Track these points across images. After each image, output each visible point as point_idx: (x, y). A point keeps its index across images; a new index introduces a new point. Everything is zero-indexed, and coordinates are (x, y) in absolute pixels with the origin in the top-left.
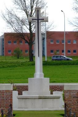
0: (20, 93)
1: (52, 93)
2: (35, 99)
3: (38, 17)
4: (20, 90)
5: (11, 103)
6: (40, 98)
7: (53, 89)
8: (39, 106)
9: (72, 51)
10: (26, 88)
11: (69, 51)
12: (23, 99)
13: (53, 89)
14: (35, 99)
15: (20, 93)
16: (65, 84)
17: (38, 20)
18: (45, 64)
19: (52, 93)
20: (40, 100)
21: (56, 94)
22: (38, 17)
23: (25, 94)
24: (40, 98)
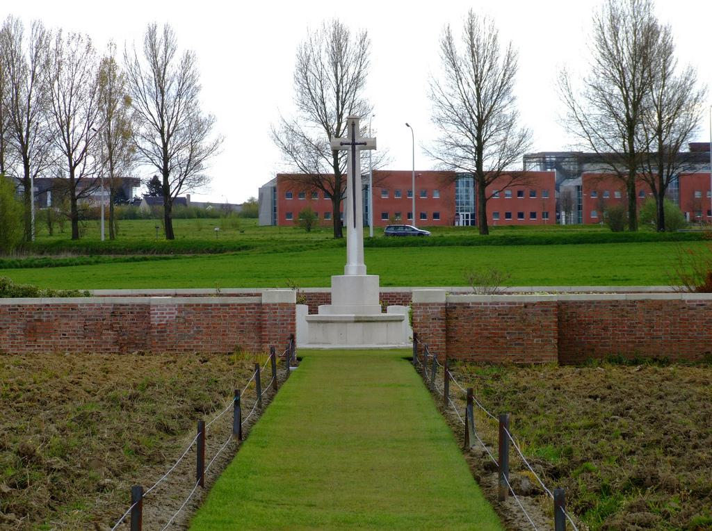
0: (313, 310)
1: (384, 310)
2: (346, 322)
4: (313, 303)
7: (387, 300)
8: (355, 339)
10: (326, 299)
11: (423, 216)
12: (319, 322)
14: (346, 322)
15: (313, 310)
17: (354, 144)
19: (384, 310)
23: (324, 312)
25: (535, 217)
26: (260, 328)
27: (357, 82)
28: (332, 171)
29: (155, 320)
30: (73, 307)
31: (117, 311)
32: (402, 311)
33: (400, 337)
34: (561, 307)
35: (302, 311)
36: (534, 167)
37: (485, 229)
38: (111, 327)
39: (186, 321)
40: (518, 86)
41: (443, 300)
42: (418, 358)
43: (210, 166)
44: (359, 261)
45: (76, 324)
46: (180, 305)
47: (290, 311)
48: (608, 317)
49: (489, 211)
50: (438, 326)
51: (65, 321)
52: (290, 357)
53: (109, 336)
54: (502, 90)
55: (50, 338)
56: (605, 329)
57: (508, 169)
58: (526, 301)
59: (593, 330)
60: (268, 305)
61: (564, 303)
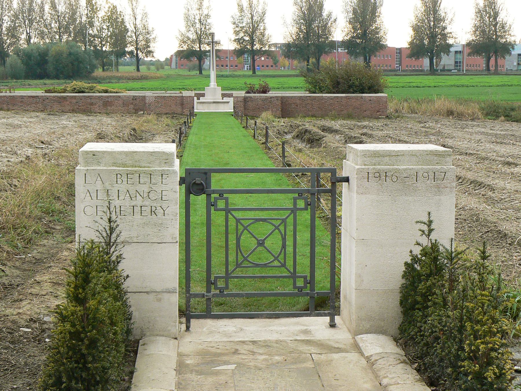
0: (198, 99)
1: (223, 99)
2: (210, 103)
3: (213, 40)
4: (199, 96)
5: (68, 178)
6: (214, 103)
7: (224, 95)
8: (213, 109)
9: (234, 65)
10: (203, 95)
11: (232, 66)
12: (201, 103)
13: (224, 95)
14: (210, 103)
15: (198, 99)
16: (43, 94)
17: (213, 42)
18: (218, 76)
19: (223, 99)
20: (148, 290)
21: (226, 99)
22: (213, 40)
23: (202, 99)
24: (214, 103)
25: (513, 337)
26: (182, 104)
27: (207, 16)
28: (198, 49)
29: (147, 101)
30: (119, 97)
31: (135, 98)
32: (231, 100)
33: (229, 108)
34: (282, 98)
35: (195, 98)
36: (273, 49)
37: (254, 72)
38: (132, 103)
39: (158, 102)
40: (268, 19)
41: (244, 96)
42: (235, 114)
43: (153, 46)
44: (214, 82)
45: (120, 102)
46: (155, 96)
47: (193, 98)
48: (298, 102)
49: (256, 65)
50: (242, 104)
51: (116, 101)
52: (192, 114)
53: (131, 106)
54: (262, 20)
55: (112, 107)
56: (297, 106)
57: (263, 49)
58: (271, 96)
59: (293, 106)
60: (185, 96)
61: (283, 97)
